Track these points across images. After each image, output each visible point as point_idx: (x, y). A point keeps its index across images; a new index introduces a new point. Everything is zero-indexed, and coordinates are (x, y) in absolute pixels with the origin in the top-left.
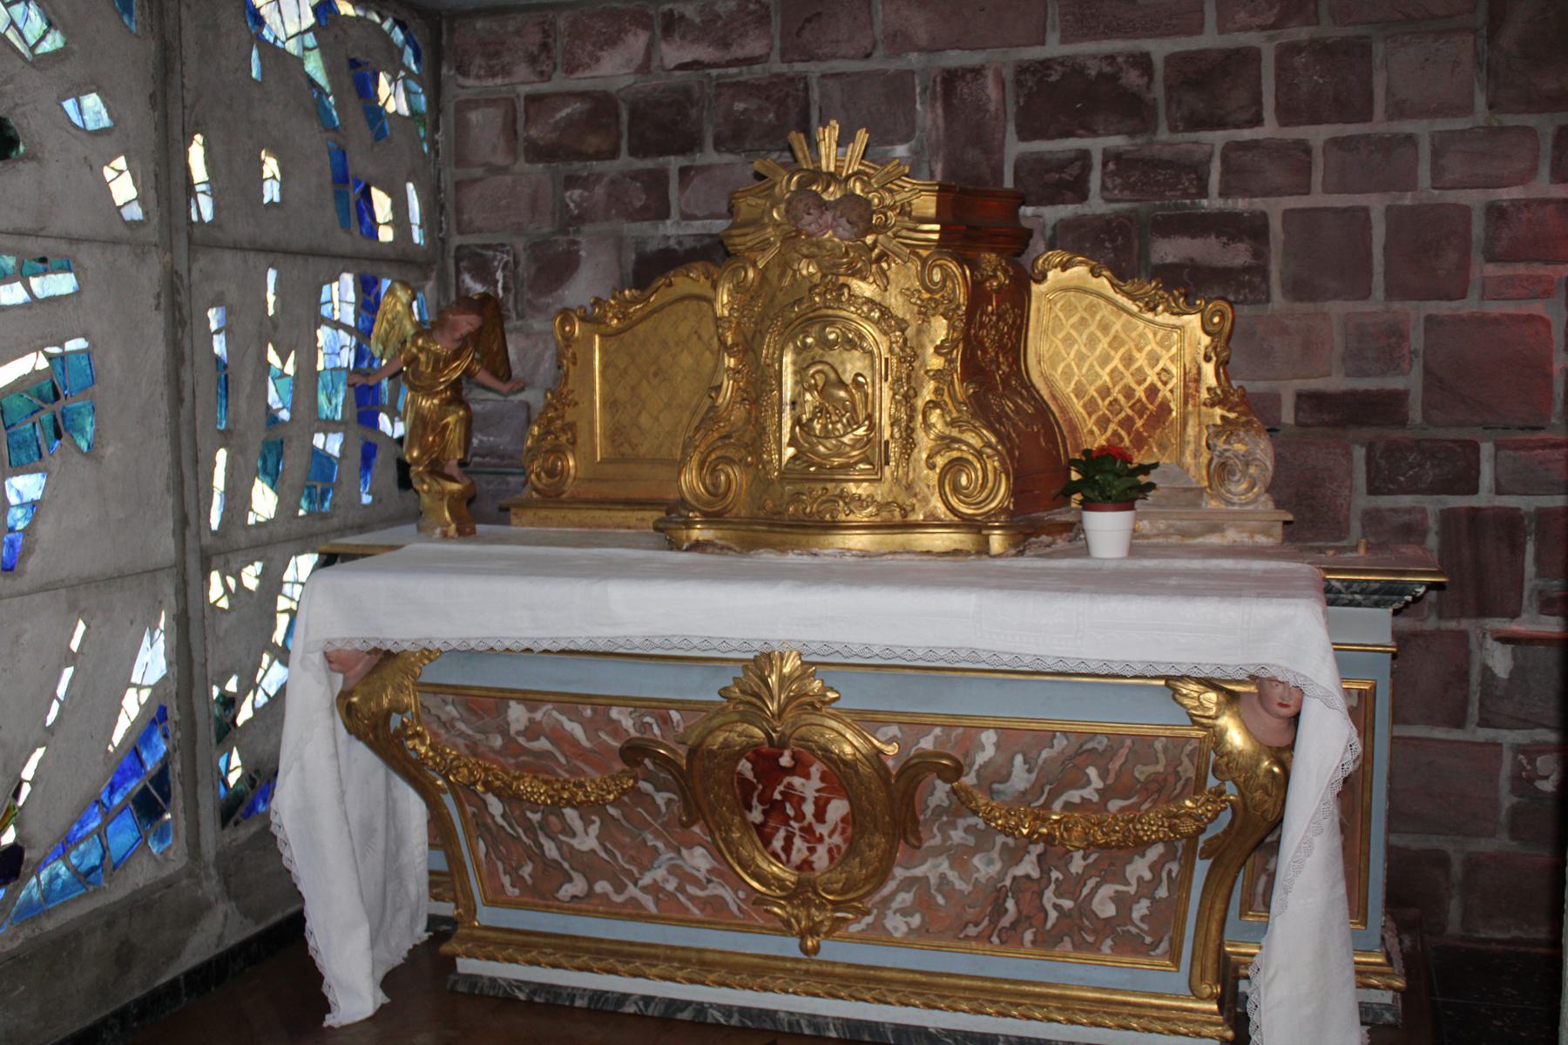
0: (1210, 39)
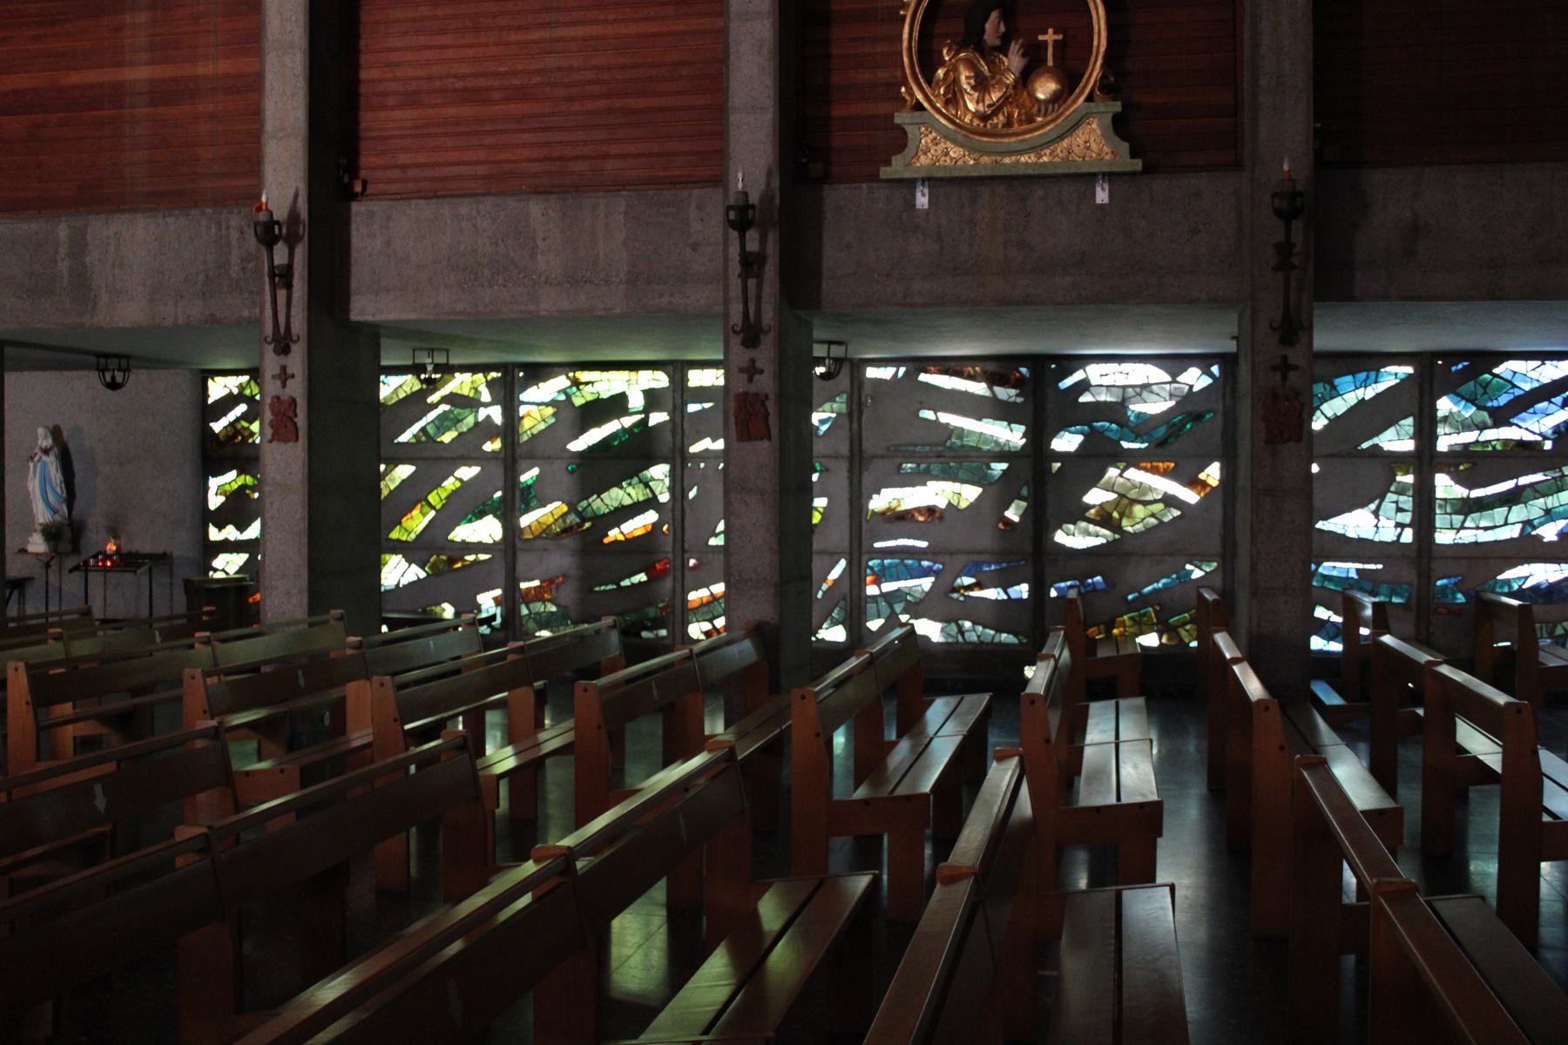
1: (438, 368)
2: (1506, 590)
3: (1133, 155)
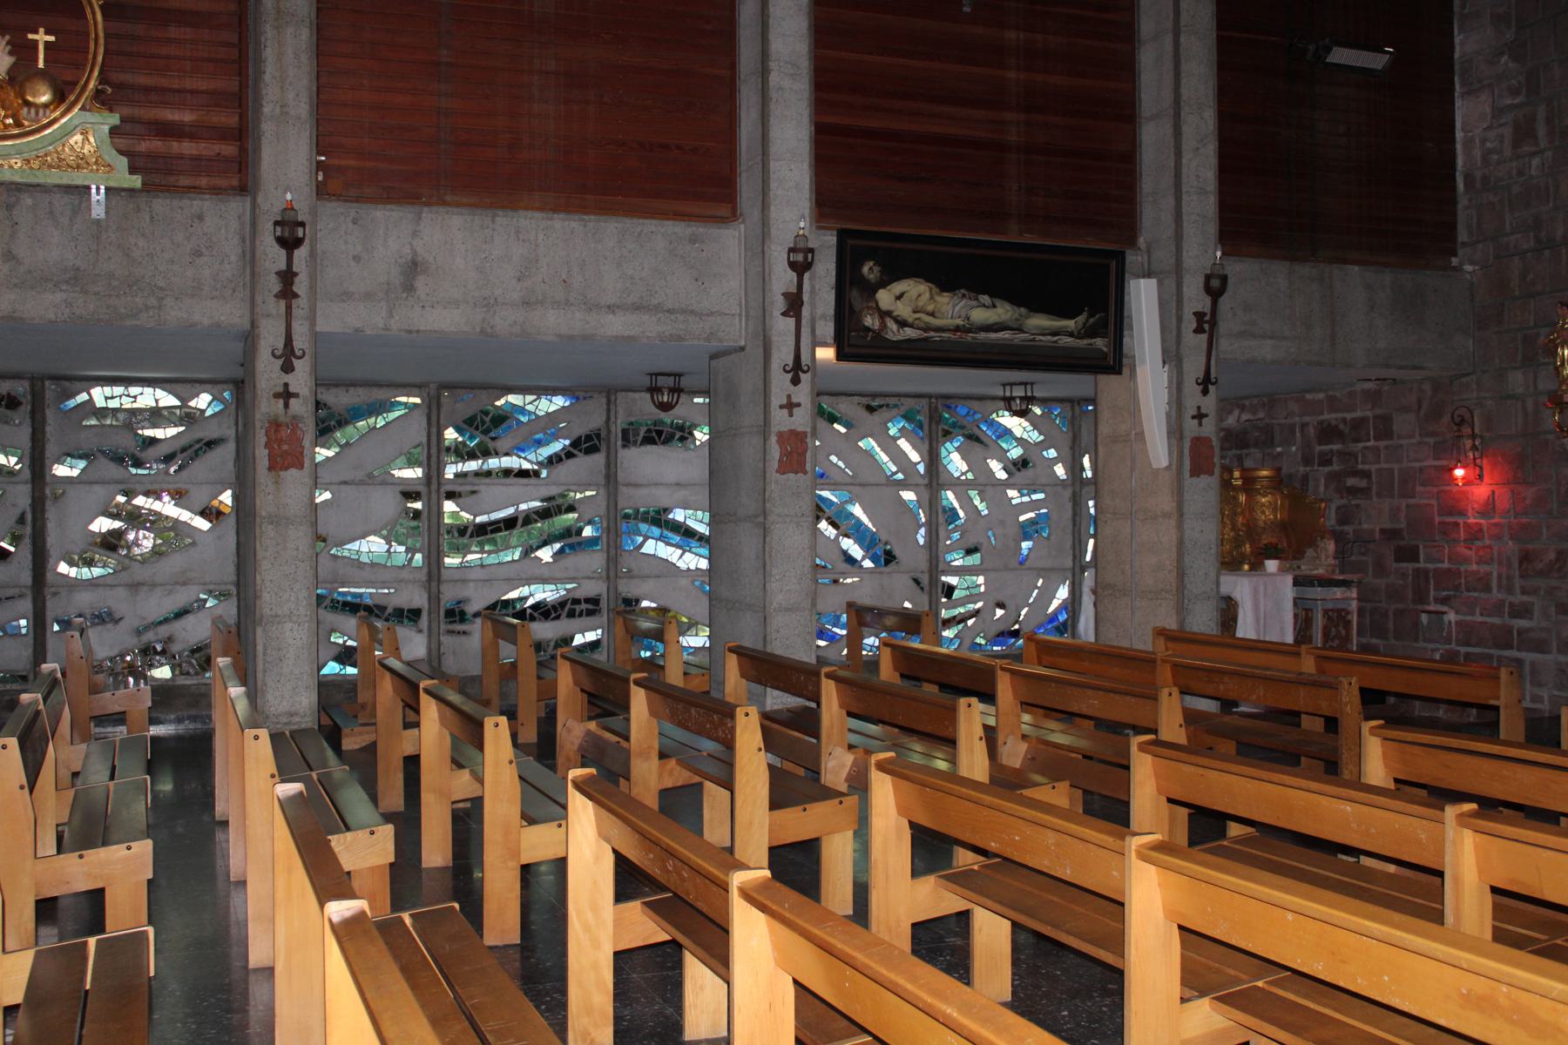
0: (1358, 414)
1: (672, 390)
2: (511, 611)
3: (133, 170)
